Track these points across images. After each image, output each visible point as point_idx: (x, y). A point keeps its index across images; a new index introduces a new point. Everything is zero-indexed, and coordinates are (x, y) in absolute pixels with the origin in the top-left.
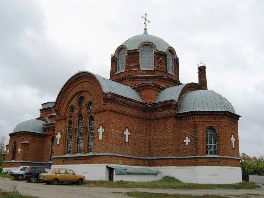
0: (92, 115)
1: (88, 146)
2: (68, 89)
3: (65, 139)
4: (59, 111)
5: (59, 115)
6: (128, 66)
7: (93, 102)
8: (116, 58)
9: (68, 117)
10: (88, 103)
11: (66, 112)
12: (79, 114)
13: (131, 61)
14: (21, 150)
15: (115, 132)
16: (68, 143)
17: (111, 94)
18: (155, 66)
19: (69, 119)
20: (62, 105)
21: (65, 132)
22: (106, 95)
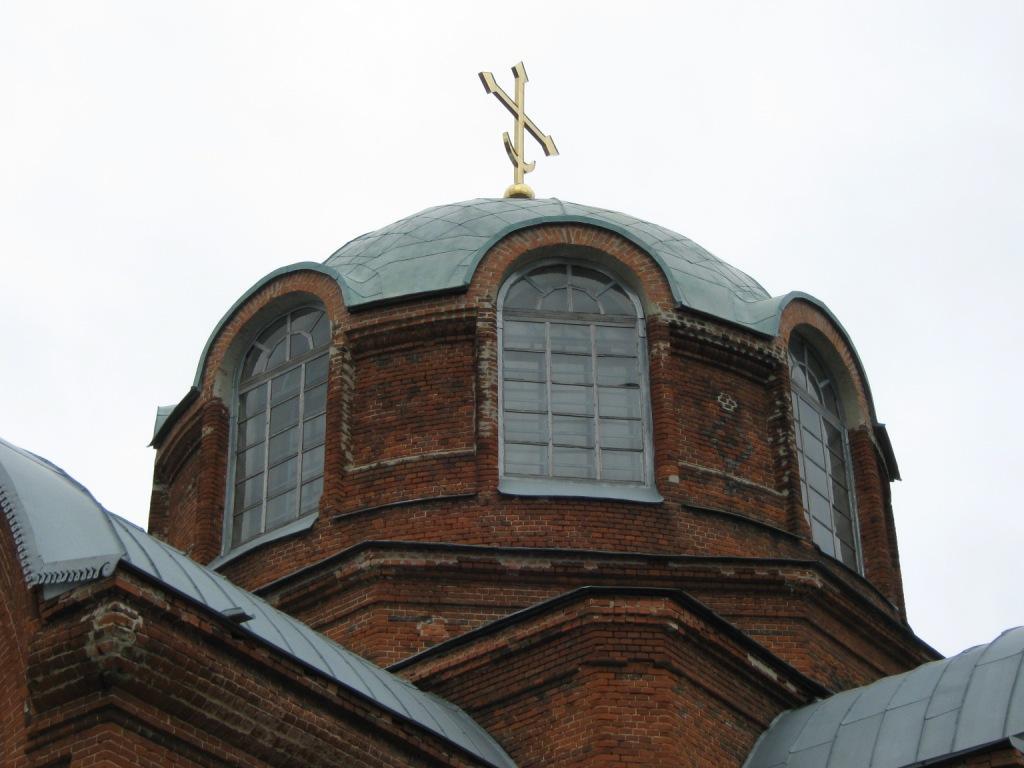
6: (351, 469)
8: (218, 414)
13: (390, 417)
17: (142, 605)
18: (659, 461)
22: (77, 608)
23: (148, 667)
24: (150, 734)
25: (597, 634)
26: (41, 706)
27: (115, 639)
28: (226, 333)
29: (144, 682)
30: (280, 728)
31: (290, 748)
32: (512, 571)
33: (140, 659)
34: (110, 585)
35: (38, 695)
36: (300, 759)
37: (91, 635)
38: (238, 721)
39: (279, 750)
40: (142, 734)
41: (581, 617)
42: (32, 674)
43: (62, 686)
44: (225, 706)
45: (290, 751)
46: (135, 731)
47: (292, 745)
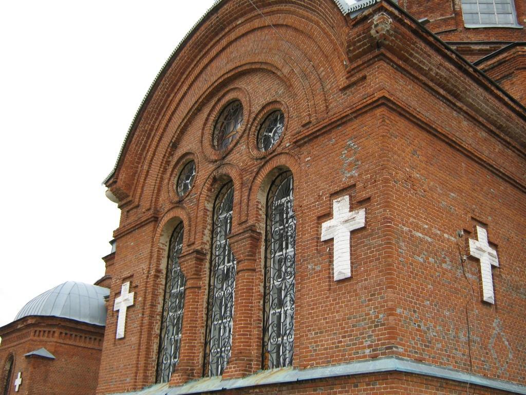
0: (282, 161)
1: (265, 330)
2: (168, 96)
3: (147, 312)
4: (131, 194)
5: (131, 212)
7: (286, 103)
9: (168, 206)
10: (257, 115)
11: (159, 190)
12: (215, 180)
13: (421, 9)
14: (22, 382)
15: (427, 233)
16: (161, 330)
17: (391, 14)
19: (171, 215)
20: (146, 167)
21: (151, 279)
22: (365, 18)
23: (394, 39)
24: (395, 66)
25: (521, 58)
26: (351, 60)
27: (383, 26)
28: (148, 299)
29: (393, 45)
30: (438, 68)
31: (441, 77)
32: (476, 50)
33: (391, 35)
34: (380, 6)
35: (351, 55)
36: (444, 81)
37: (373, 26)
38: (424, 64)
39: (437, 77)
40: (392, 66)
41: (514, 54)
42: (349, 46)
43: (361, 50)
44: (420, 57)
45: (441, 78)
46: (390, 64)
47: (442, 75)
